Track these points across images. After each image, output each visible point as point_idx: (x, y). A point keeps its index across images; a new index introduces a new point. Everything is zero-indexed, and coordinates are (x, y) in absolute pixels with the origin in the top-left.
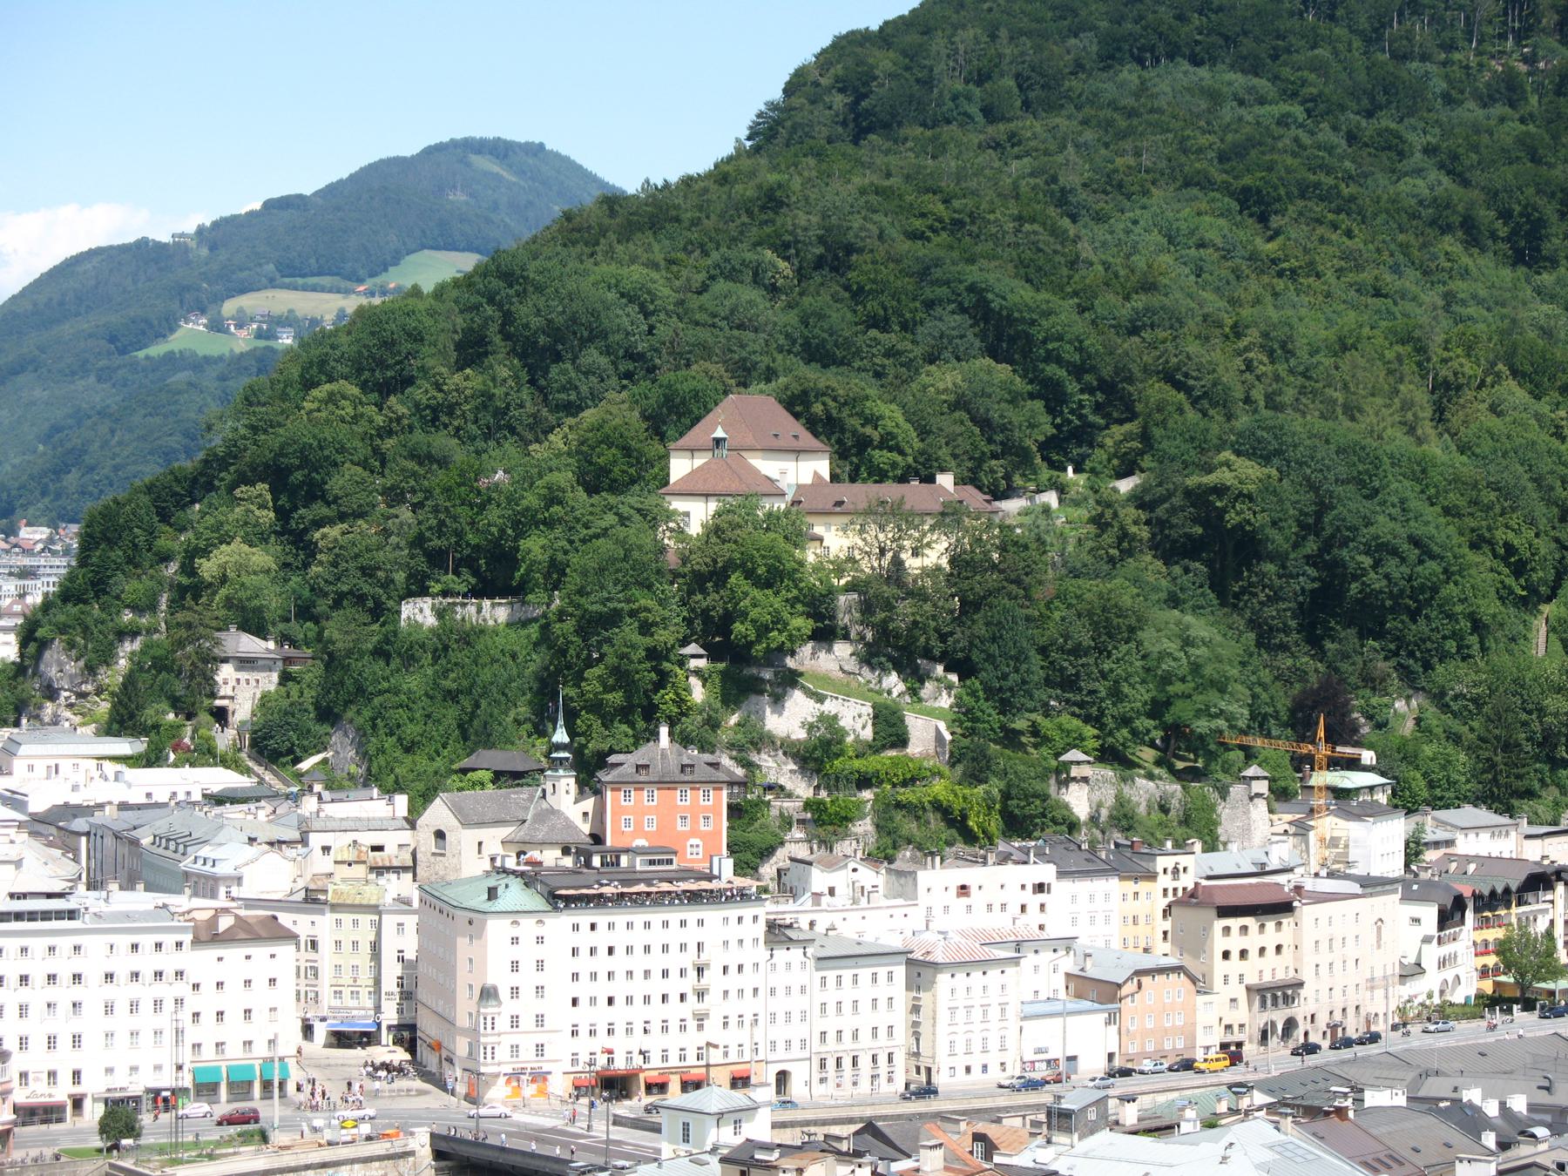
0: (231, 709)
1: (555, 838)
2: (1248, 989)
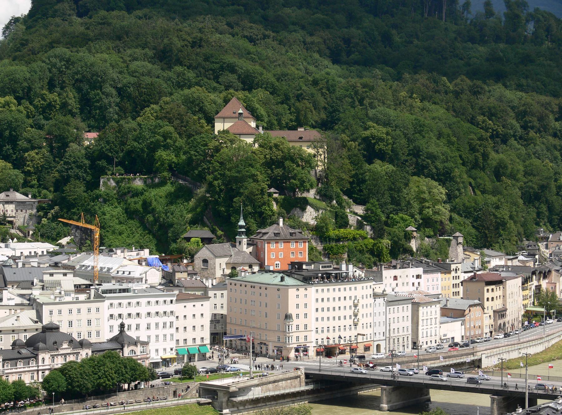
0: (14, 221)
1: (246, 262)
2: (494, 311)
